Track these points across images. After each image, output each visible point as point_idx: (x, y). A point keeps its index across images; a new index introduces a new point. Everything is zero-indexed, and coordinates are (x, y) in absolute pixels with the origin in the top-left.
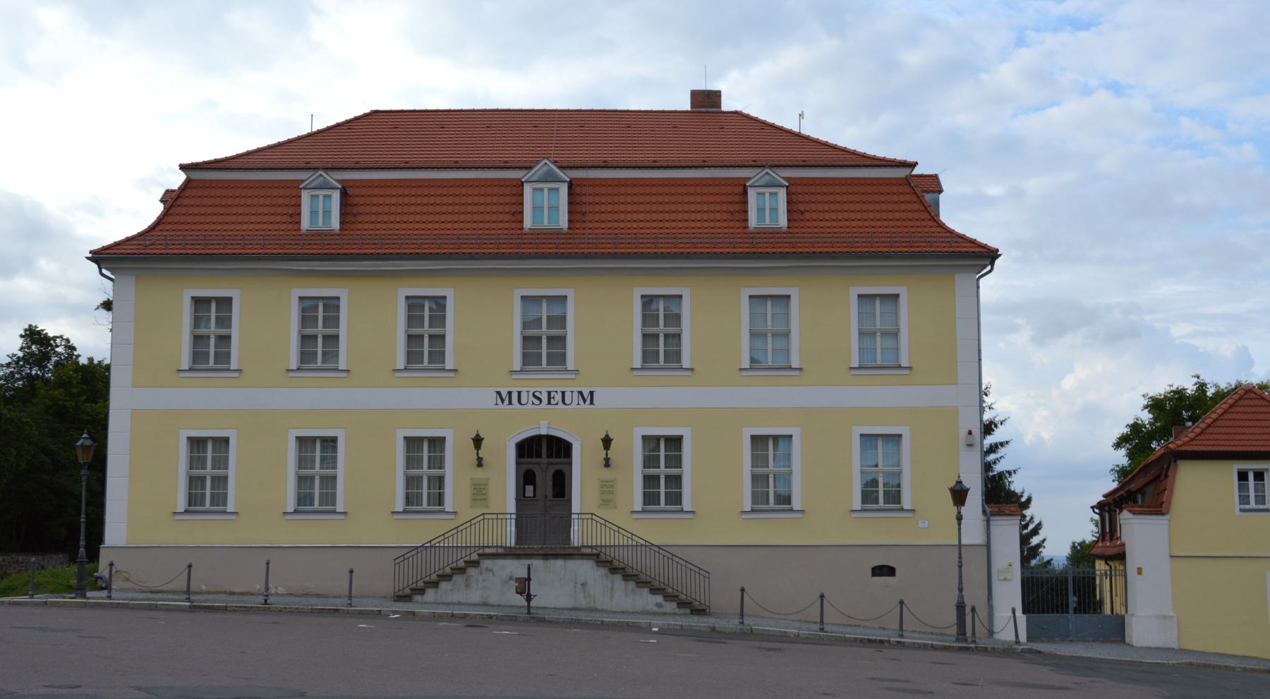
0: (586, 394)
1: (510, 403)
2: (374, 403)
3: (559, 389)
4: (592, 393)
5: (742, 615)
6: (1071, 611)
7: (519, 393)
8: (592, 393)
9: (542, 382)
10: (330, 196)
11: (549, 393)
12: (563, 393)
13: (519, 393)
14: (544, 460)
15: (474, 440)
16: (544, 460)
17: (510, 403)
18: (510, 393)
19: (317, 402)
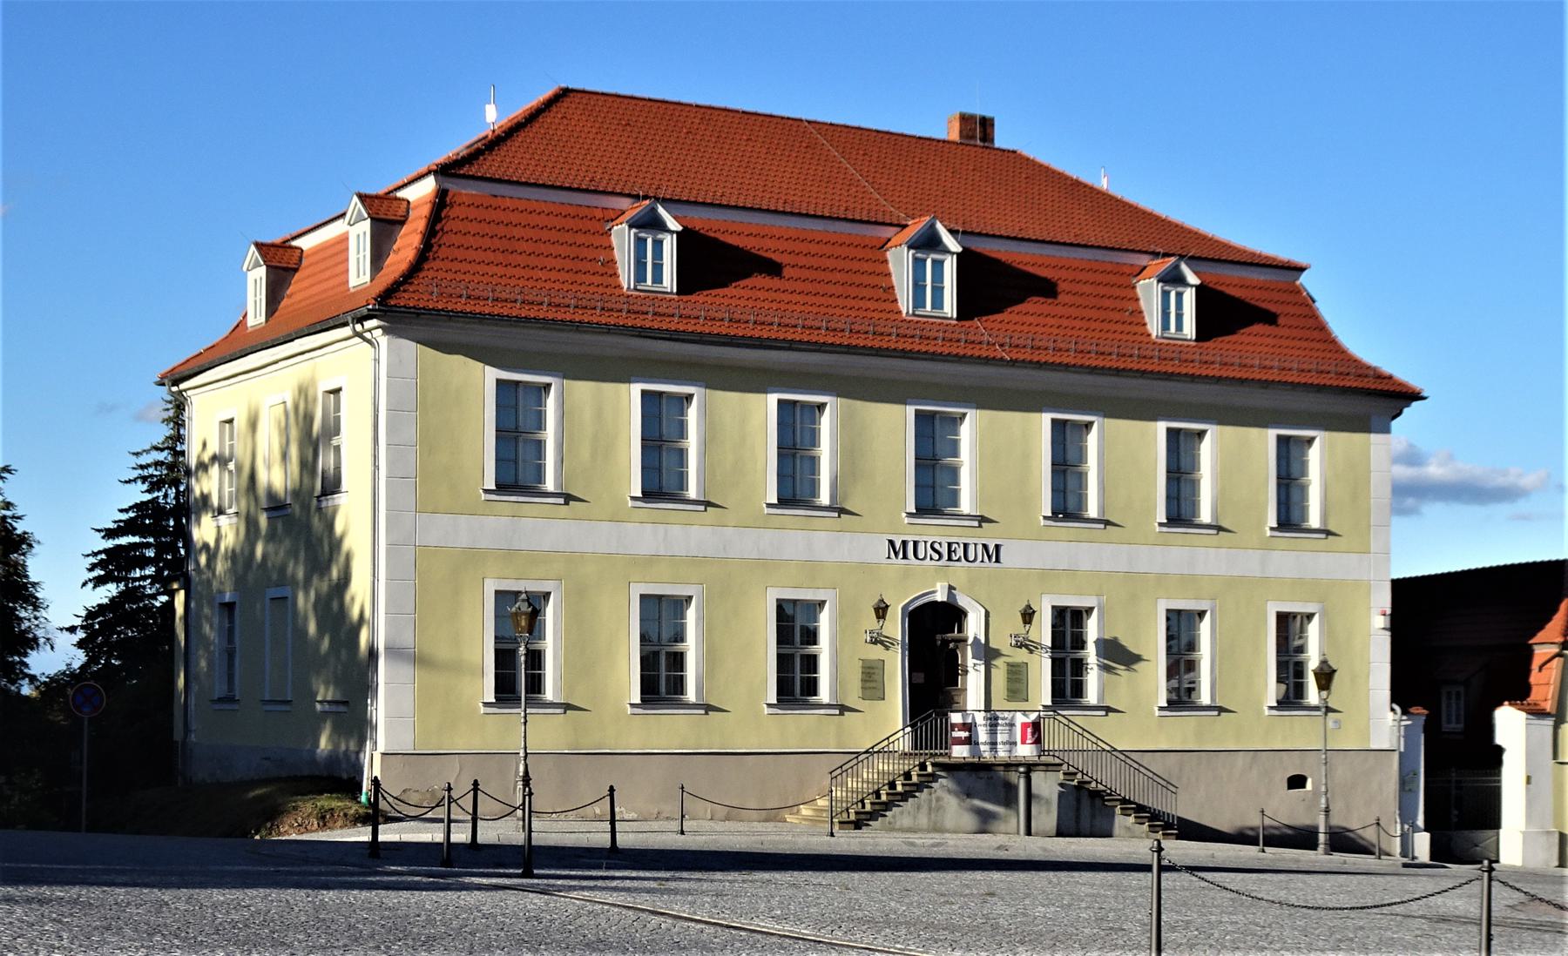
0: (991, 548)
1: (905, 557)
2: (738, 554)
3: (962, 540)
4: (997, 547)
5: (613, 822)
6: (1321, 847)
7: (916, 543)
8: (997, 547)
9: (933, 531)
10: (942, 263)
11: (950, 545)
12: (966, 546)
13: (916, 543)
14: (933, 636)
15: (877, 610)
16: (933, 636)
17: (905, 557)
18: (904, 543)
19: (809, 554)
